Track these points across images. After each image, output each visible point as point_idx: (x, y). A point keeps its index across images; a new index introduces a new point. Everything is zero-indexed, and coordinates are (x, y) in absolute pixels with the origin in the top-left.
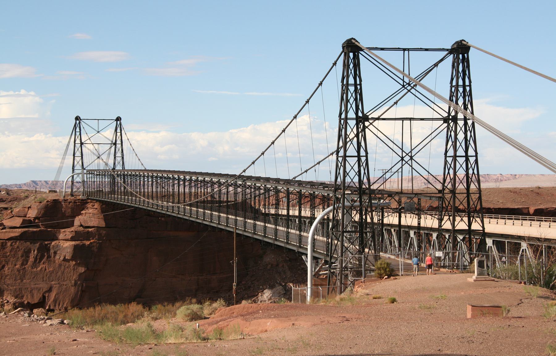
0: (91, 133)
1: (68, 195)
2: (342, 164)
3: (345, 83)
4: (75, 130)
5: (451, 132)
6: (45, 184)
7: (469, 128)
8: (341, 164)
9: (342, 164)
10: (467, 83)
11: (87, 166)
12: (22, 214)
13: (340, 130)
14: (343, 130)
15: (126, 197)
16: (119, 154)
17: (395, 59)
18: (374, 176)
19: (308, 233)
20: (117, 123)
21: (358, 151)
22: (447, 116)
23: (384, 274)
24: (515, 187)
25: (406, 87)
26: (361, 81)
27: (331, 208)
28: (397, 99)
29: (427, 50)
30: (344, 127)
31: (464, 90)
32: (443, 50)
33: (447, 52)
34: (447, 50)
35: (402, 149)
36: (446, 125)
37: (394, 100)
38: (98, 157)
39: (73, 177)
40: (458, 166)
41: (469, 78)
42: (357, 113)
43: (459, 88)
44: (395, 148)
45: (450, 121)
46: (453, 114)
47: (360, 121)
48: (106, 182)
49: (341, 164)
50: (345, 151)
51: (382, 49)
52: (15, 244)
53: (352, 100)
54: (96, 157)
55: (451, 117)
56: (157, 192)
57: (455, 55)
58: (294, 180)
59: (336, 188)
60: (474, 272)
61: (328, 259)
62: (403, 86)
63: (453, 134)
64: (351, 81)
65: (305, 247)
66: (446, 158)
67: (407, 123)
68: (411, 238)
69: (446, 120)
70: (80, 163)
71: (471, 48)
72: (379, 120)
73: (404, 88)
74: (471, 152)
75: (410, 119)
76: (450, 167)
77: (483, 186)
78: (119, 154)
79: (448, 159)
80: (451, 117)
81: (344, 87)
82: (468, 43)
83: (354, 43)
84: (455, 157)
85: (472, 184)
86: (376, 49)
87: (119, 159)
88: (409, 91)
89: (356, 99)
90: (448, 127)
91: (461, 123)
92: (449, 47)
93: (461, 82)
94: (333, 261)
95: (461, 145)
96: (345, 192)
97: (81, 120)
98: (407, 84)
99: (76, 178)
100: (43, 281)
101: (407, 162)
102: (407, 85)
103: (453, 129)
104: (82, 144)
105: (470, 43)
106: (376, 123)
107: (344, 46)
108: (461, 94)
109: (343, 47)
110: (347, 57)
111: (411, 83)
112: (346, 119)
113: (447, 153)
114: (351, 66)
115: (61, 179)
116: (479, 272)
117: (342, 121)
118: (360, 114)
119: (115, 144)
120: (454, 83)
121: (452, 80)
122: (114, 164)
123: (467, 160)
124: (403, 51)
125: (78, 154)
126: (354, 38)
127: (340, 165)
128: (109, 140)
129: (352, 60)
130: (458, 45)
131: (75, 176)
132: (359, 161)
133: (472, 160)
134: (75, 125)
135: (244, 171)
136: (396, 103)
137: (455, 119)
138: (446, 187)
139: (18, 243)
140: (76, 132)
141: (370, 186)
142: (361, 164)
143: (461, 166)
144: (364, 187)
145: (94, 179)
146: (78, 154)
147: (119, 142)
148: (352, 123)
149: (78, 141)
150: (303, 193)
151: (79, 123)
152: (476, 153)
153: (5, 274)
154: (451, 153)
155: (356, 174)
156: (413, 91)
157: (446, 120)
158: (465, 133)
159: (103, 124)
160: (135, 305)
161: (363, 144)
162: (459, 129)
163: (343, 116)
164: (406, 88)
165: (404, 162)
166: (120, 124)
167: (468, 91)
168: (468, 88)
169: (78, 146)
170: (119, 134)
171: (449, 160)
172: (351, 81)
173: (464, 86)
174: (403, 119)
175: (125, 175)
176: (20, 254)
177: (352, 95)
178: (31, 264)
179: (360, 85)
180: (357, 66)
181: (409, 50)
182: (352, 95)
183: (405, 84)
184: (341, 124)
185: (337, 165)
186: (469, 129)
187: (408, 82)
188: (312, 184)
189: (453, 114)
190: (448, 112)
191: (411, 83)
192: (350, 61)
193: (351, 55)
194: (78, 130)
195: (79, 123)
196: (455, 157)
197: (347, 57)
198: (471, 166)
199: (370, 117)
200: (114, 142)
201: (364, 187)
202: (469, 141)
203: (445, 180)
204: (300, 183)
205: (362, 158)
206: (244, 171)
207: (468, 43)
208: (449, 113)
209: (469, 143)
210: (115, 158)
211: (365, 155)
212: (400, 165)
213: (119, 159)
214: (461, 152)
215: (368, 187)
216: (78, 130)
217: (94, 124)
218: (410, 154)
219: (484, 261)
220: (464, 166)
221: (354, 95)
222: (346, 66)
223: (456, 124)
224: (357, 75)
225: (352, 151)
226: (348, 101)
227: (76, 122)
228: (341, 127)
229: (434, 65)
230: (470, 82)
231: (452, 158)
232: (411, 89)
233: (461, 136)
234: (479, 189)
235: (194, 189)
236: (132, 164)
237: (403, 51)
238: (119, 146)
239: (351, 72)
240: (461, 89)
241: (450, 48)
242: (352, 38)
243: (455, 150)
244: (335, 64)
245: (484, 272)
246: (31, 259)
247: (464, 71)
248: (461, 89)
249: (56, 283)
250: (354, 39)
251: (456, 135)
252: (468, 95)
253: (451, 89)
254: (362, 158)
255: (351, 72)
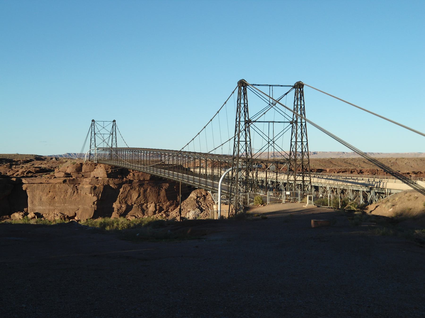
0: (100, 128)
1: (88, 161)
2: (237, 145)
3: (239, 102)
4: (92, 127)
5: (294, 129)
6: (74, 154)
7: (303, 127)
8: (237, 145)
9: (237, 145)
10: (302, 103)
11: (98, 146)
12: (64, 171)
13: (236, 127)
14: (238, 127)
15: (120, 162)
16: (114, 140)
17: (266, 90)
18: (254, 152)
19: (219, 182)
20: (113, 123)
21: (246, 139)
22: (292, 120)
23: (259, 204)
24: (5, 154)
25: (271, 105)
26: (247, 101)
27: (231, 169)
28: (265, 112)
29: (282, 86)
30: (238, 126)
31: (301, 107)
32: (290, 86)
33: (292, 87)
34: (292, 86)
35: (268, 138)
36: (291, 125)
37: (264, 112)
38: (104, 141)
39: (90, 151)
40: (298, 147)
41: (304, 101)
42: (245, 119)
43: (298, 106)
44: (264, 136)
45: (294, 123)
46: (295, 119)
47: (247, 123)
48: (108, 154)
49: (237, 145)
50: (239, 138)
51: (258, 85)
52: (60, 186)
53: (242, 112)
54: (103, 141)
55: (294, 121)
56: (132, 159)
57: (296, 89)
58: (209, 153)
59: (233, 158)
60: (306, 203)
61: (229, 196)
62: (270, 105)
63: (295, 130)
64: (242, 101)
65: (216, 189)
66: (235, 142)
67: (271, 124)
68: (269, 184)
69: (291, 123)
70: (94, 144)
71: (304, 85)
72: (255, 122)
73: (270, 106)
74: (304, 140)
75: (273, 122)
76: (294, 147)
77: (310, 157)
78: (114, 140)
79: (292, 143)
80: (294, 121)
81: (238, 105)
82: (303, 83)
83: (244, 82)
84: (296, 142)
85: (305, 156)
86: (255, 85)
87: (114, 142)
88: (272, 107)
89: (244, 111)
90: (293, 126)
91: (299, 124)
92: (293, 85)
93: (299, 103)
94: (232, 196)
95: (299, 136)
96: (238, 160)
97: (95, 121)
98: (271, 103)
99: (92, 152)
100: (75, 205)
101: (271, 145)
102: (272, 104)
103: (295, 127)
104: (95, 134)
105: (304, 83)
106: (254, 123)
107: (238, 83)
108: (299, 109)
109: (238, 84)
110: (240, 89)
111: (273, 103)
112: (240, 121)
113: (292, 140)
114: (242, 93)
115: (84, 152)
116: (309, 203)
117: (237, 123)
118: (247, 119)
119: (112, 134)
120: (296, 104)
121: (295, 101)
122: (112, 145)
123: (302, 144)
124: (269, 86)
125: (93, 139)
126: (244, 79)
127: (236, 146)
128: (109, 132)
129: (242, 91)
130: (298, 84)
131: (91, 151)
132: (246, 143)
133: (305, 144)
134: (92, 124)
135: (183, 148)
136: (264, 113)
137: (296, 122)
138: (291, 158)
139: (62, 185)
140: (92, 128)
141: (252, 156)
142: (247, 146)
143: (299, 147)
144: (248, 157)
145: (100, 152)
146: (93, 139)
147: (114, 133)
148: (243, 124)
149: (93, 133)
150: (208, 160)
151: (94, 123)
152: (307, 140)
153: (55, 201)
154: (294, 140)
155: (245, 150)
156: (274, 107)
157: (291, 123)
158: (301, 130)
159: (106, 124)
160: (123, 218)
161: (248, 134)
162: (298, 127)
163: (238, 120)
164: (271, 106)
165: (269, 144)
166: (115, 123)
167: (303, 108)
168: (303, 106)
169: (93, 135)
170: (114, 129)
171: (236, 143)
172: (242, 101)
173: (301, 105)
174: (269, 122)
175: (117, 150)
176: (63, 190)
177: (243, 109)
178: (69, 196)
179: (247, 103)
180: (245, 94)
181: (272, 86)
182: (243, 109)
183: (270, 103)
184: (237, 124)
185: (234, 146)
186: (303, 128)
187: (272, 103)
188: (219, 156)
189: (295, 119)
190: (292, 118)
191: (273, 103)
192: (242, 91)
193: (242, 88)
194: (93, 127)
195: (94, 123)
196: (296, 142)
197: (240, 89)
198: (304, 147)
199: (252, 120)
200: (112, 133)
201: (248, 157)
202: (303, 134)
203: (291, 154)
204: (213, 155)
205: (247, 142)
206: (183, 148)
207: (303, 83)
208: (293, 120)
209: (303, 135)
210: (112, 141)
211: (249, 141)
212: (271, 138)
213: (114, 142)
214: (299, 140)
215: (251, 157)
216: (93, 127)
217: (101, 124)
218: (273, 140)
219: (312, 197)
220: (301, 147)
221: (243, 109)
222: (239, 94)
223: (297, 124)
224: (245, 98)
225: (242, 138)
226: (240, 112)
227: (92, 123)
228: (237, 125)
229: (285, 94)
230: (304, 103)
231: (237, 142)
232: (273, 106)
233: (299, 131)
234: (308, 158)
235: (151, 158)
236: (121, 145)
237: (269, 86)
238: (114, 135)
239: (242, 97)
240: (299, 107)
241: (294, 85)
242: (243, 79)
243: (296, 139)
244: (233, 92)
245: (312, 203)
246: (69, 194)
247: (301, 97)
248: (299, 107)
249: (82, 206)
250: (244, 80)
251: (297, 130)
252: (303, 110)
253: (294, 106)
254: (247, 142)
255: (242, 97)
